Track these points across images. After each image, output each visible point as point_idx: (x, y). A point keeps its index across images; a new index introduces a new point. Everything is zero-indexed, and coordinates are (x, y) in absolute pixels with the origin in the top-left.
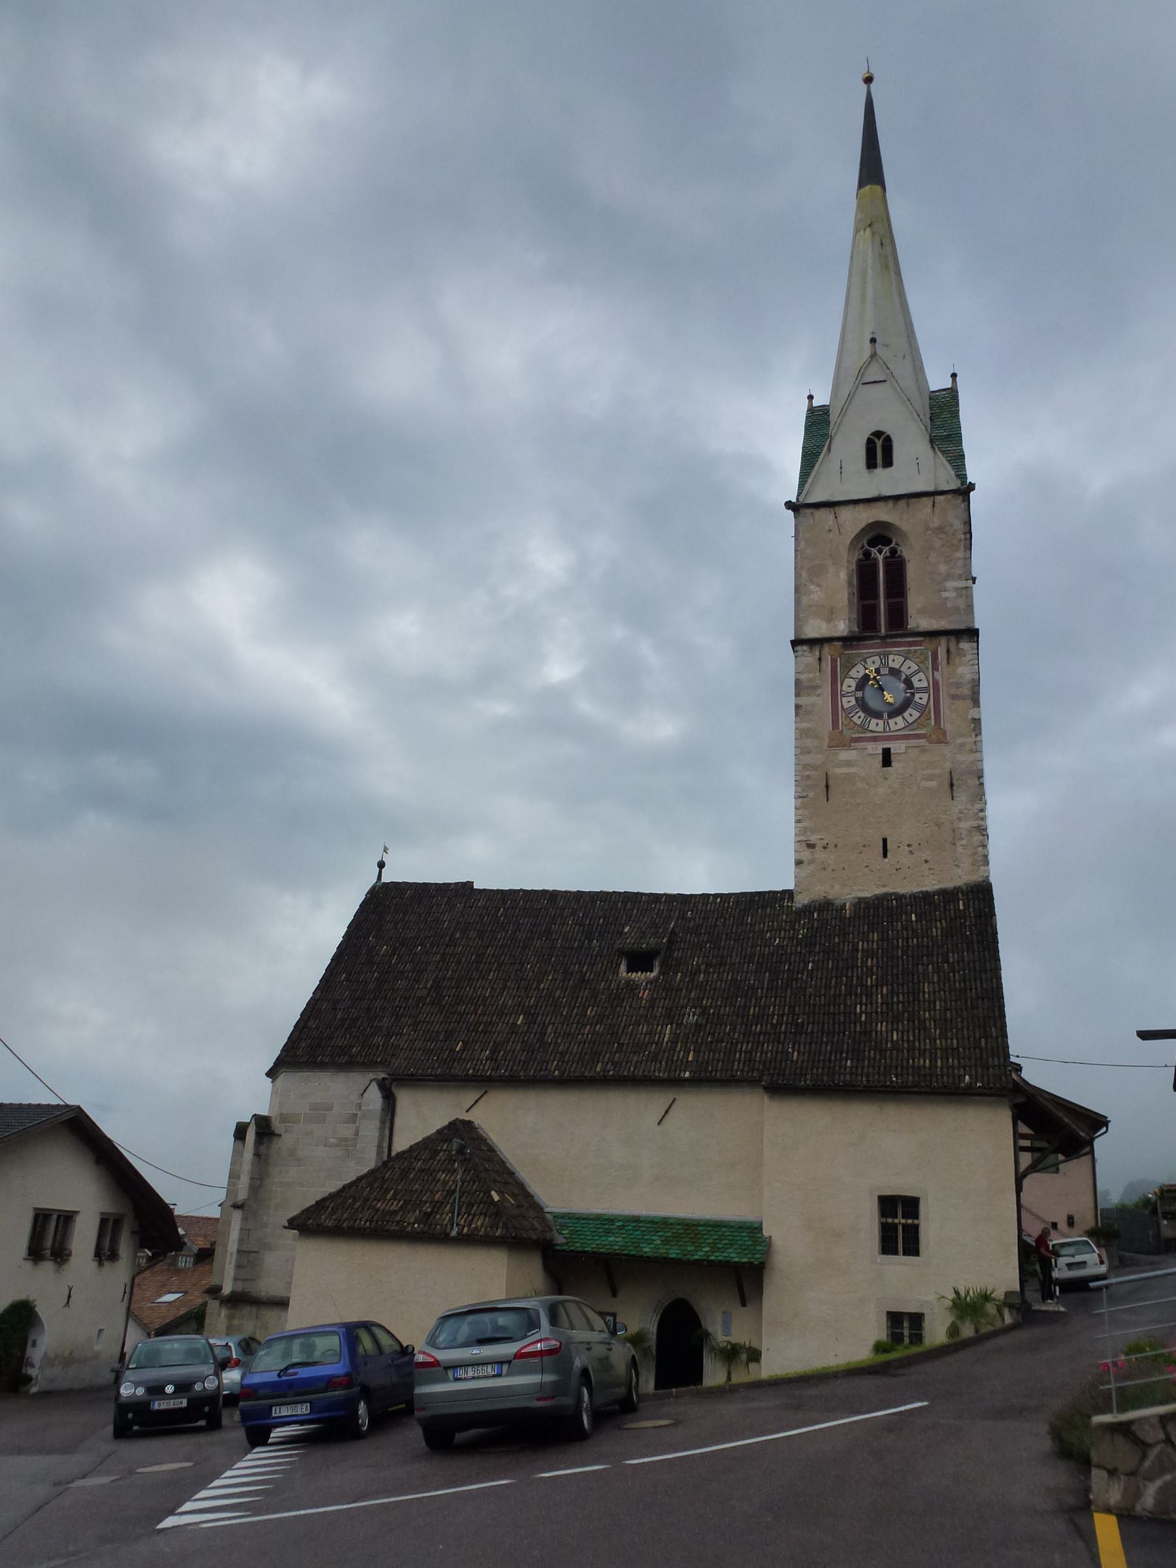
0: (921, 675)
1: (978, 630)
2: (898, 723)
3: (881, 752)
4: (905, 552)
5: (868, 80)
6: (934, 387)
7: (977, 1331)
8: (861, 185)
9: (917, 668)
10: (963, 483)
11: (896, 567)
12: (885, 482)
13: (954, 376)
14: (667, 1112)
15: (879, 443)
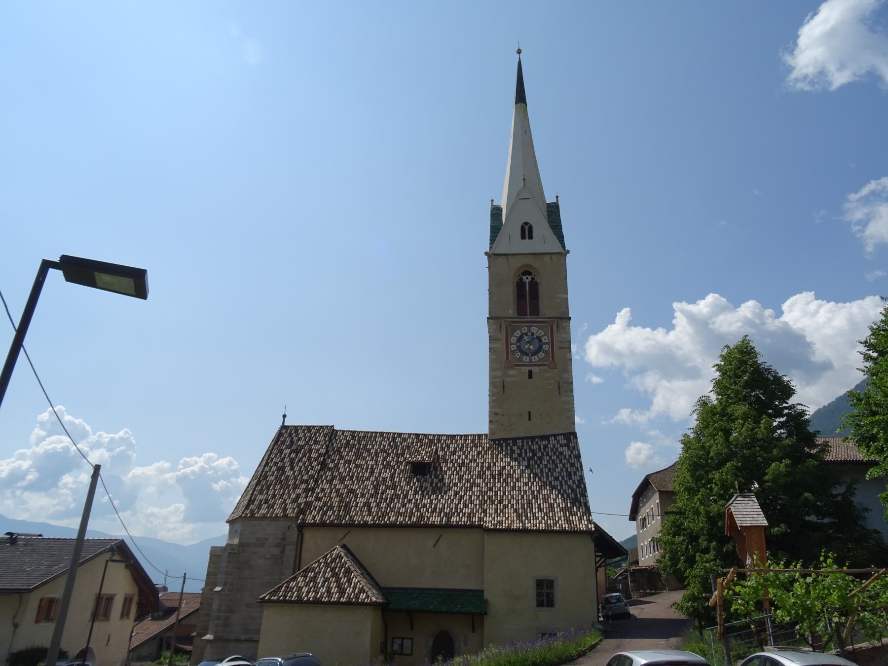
0: (546, 337)
1: (571, 317)
2: (535, 359)
3: (528, 371)
4: (537, 279)
5: (519, 52)
6: (548, 201)
8: (516, 103)
9: (544, 333)
10: (565, 249)
11: (534, 285)
12: (527, 246)
13: (557, 197)
14: (438, 541)
15: (527, 228)
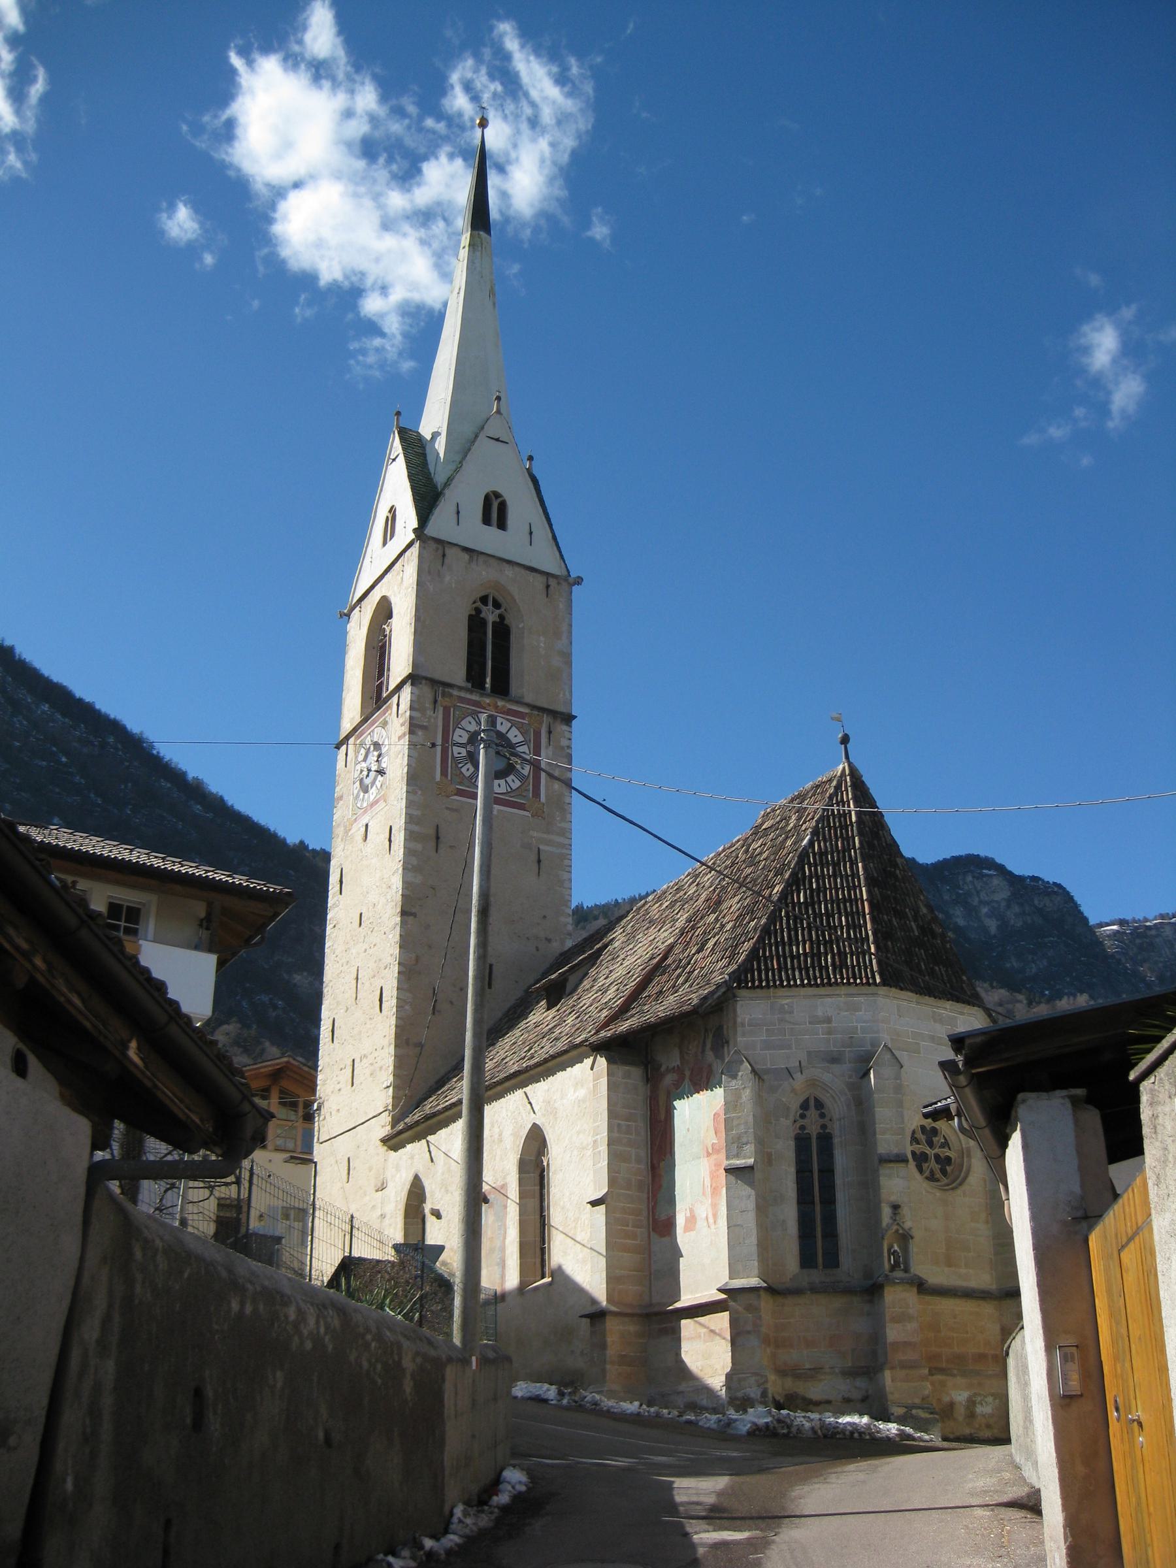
11: (503, 632)
12: (488, 539)
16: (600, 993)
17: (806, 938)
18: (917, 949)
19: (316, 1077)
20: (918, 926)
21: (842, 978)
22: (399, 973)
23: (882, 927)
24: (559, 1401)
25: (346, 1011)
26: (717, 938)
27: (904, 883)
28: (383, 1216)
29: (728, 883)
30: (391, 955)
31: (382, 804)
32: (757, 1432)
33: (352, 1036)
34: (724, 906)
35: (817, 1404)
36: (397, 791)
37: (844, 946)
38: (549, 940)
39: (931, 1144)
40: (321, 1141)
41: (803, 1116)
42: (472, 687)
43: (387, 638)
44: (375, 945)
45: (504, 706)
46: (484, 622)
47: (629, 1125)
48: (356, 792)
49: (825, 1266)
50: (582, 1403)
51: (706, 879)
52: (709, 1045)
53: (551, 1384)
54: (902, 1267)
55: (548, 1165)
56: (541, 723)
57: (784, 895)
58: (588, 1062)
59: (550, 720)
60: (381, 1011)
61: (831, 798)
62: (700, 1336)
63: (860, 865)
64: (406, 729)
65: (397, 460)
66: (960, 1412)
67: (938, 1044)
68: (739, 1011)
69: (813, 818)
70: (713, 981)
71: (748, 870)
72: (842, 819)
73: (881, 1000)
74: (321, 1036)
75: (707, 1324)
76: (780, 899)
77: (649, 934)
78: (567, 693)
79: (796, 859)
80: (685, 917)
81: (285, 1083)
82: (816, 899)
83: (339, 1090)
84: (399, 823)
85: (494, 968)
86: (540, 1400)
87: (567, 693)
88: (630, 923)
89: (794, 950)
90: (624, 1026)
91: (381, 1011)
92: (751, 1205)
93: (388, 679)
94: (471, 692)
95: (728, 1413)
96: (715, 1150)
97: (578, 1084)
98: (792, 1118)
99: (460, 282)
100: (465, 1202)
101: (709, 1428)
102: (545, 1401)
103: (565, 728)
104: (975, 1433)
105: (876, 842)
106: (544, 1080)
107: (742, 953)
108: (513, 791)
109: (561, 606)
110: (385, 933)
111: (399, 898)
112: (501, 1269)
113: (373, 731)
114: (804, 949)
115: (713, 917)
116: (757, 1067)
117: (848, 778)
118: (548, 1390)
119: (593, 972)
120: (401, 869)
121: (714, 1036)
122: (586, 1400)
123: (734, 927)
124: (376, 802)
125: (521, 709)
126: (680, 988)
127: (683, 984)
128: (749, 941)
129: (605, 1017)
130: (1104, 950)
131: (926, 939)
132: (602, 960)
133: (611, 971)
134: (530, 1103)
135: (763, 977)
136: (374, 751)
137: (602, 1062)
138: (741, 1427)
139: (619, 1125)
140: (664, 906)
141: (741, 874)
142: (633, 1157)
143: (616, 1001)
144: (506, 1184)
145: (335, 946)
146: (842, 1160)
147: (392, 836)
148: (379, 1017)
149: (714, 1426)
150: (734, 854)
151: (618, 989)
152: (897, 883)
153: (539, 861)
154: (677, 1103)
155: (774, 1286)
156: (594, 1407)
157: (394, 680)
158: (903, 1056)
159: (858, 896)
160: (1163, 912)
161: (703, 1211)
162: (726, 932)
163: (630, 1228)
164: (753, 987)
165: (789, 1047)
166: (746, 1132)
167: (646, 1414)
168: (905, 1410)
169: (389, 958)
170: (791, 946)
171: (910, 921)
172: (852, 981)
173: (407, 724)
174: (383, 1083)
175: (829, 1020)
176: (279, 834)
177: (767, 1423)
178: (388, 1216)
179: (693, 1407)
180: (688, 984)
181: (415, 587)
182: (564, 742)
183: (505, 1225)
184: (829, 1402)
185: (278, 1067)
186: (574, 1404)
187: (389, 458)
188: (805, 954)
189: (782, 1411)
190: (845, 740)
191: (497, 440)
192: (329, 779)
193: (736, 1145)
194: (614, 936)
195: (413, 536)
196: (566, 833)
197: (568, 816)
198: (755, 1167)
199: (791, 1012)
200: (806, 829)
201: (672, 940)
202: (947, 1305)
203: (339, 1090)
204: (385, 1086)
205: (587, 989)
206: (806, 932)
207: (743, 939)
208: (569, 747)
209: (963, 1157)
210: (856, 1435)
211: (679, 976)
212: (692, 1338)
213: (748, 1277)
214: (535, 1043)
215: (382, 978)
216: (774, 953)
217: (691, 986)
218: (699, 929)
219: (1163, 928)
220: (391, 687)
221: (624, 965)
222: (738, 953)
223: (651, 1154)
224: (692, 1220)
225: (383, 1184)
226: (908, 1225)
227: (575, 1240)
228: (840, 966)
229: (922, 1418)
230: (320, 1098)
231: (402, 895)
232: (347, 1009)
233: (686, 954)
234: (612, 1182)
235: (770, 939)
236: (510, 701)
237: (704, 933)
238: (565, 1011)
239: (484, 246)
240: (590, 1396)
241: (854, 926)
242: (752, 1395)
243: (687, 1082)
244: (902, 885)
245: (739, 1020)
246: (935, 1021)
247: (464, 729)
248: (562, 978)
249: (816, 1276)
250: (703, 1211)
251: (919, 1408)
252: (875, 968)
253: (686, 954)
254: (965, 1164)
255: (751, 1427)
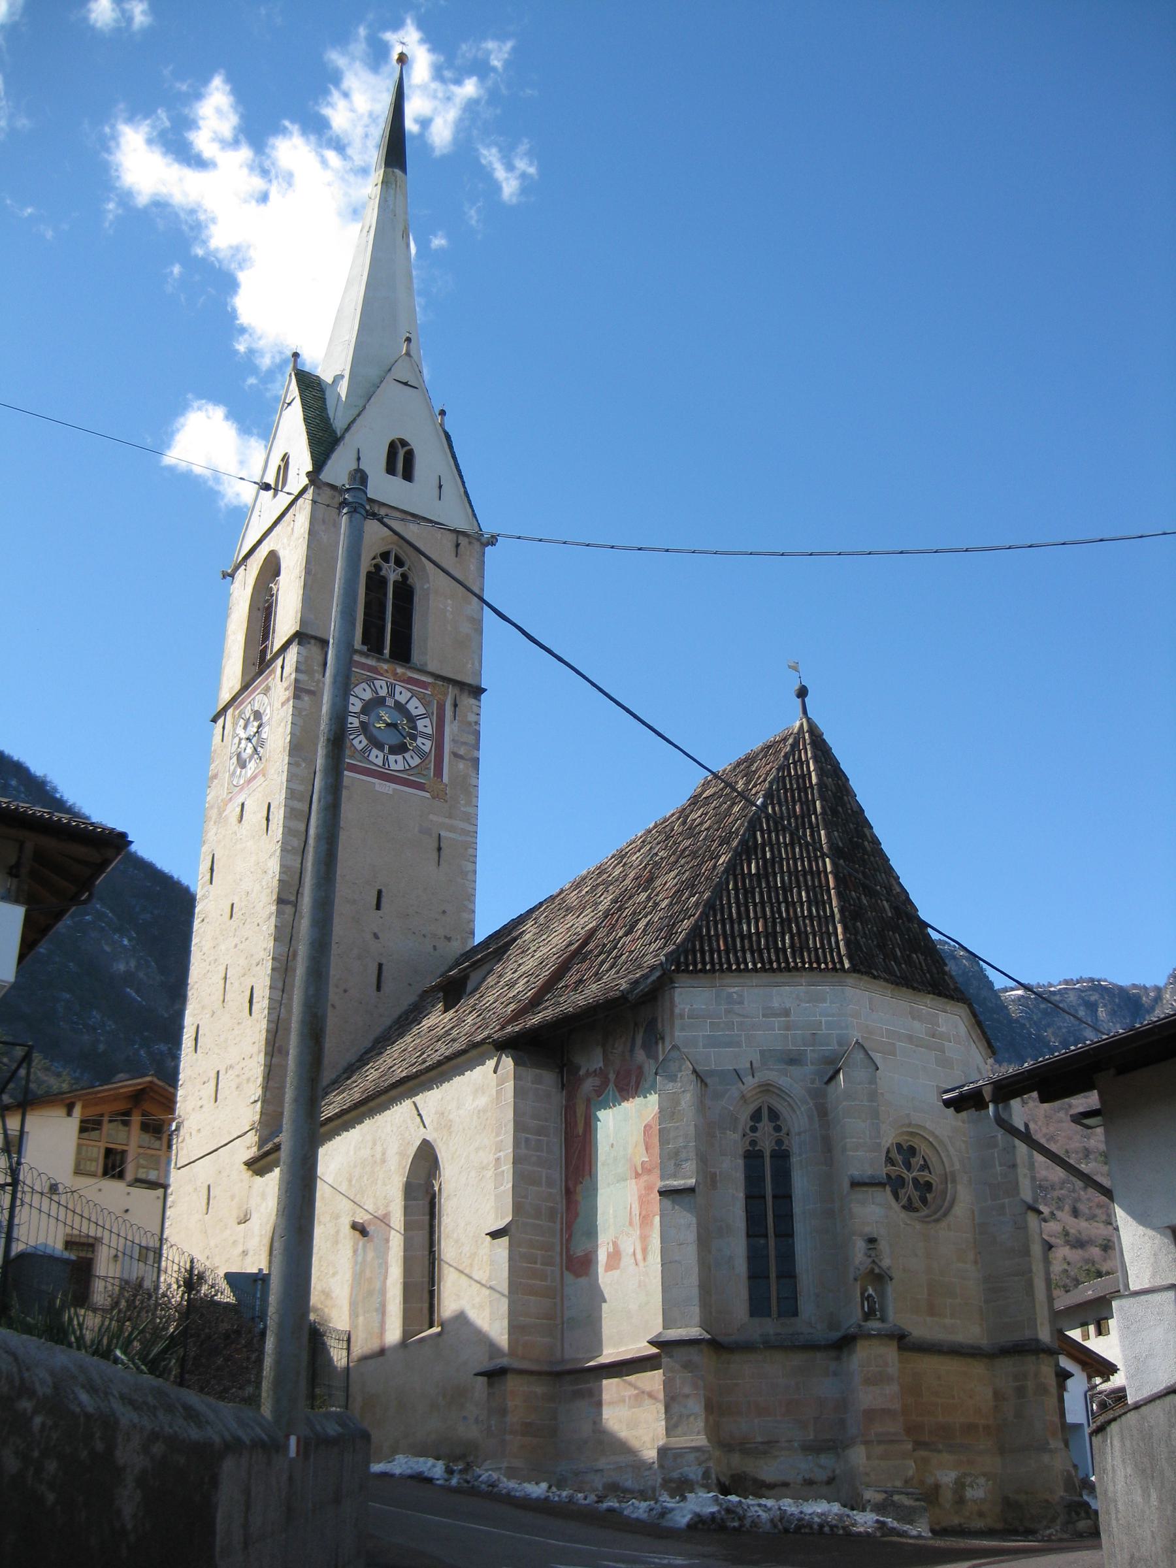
7: (99, 1277)
11: (405, 594)
15: (401, 453)
16: (507, 987)
17: (759, 914)
18: (891, 933)
19: (174, 1095)
20: (890, 906)
21: (804, 963)
22: (273, 969)
23: (850, 905)
24: (446, 1480)
25: (212, 1016)
26: (649, 917)
27: (875, 858)
28: (245, 1253)
29: (662, 858)
30: (265, 949)
31: (260, 779)
32: (700, 1526)
33: (217, 1045)
34: (658, 883)
35: (771, 1486)
36: (278, 763)
37: (805, 926)
38: (449, 939)
39: (909, 1167)
40: (178, 1166)
41: (754, 1129)
42: (368, 650)
43: (274, 597)
44: (246, 939)
45: (404, 674)
46: (383, 581)
47: (539, 1140)
48: (232, 768)
49: (780, 1315)
50: (476, 1483)
51: (634, 858)
52: (639, 1042)
53: (438, 1459)
54: (878, 1316)
55: (440, 1189)
56: (446, 694)
57: (732, 868)
58: (491, 1064)
59: (457, 691)
60: (251, 1014)
61: (786, 757)
62: (624, 1401)
63: (822, 832)
64: (290, 693)
65: (292, 404)
66: (947, 1496)
67: (917, 1046)
68: (677, 999)
69: (765, 781)
70: (645, 965)
71: (687, 843)
72: (801, 781)
73: (849, 991)
74: (183, 1046)
75: (639, 1384)
76: (726, 871)
77: (566, 922)
78: (477, 664)
79: (746, 824)
80: (609, 899)
81: (147, 1106)
82: (770, 870)
83: (201, 1107)
84: (279, 799)
85: (384, 968)
86: (422, 1479)
87: (477, 664)
88: (542, 914)
89: (745, 928)
90: (535, 1020)
91: (251, 1014)
92: (691, 1236)
93: (273, 642)
94: (367, 656)
95: (661, 1499)
96: (647, 1169)
97: (478, 1090)
98: (740, 1132)
99: (372, 218)
100: (288, 1183)
101: (637, 1519)
102: (429, 1480)
103: (473, 701)
104: (964, 1524)
105: (840, 809)
106: (438, 1088)
107: (681, 932)
108: (411, 768)
109: (472, 567)
110: (258, 925)
111: (276, 883)
112: (380, 1316)
113: (254, 699)
114: (757, 927)
115: (644, 896)
116: (698, 1068)
117: (807, 735)
118: (434, 1466)
119: (498, 968)
120: (279, 851)
121: (645, 1031)
122: (480, 1479)
123: (670, 904)
124: (254, 778)
125: (424, 678)
126: (604, 975)
127: (607, 971)
128: (689, 919)
129: (512, 1011)
130: (1008, 1014)
131: (900, 921)
132: (510, 955)
133: (520, 965)
134: (419, 1115)
135: (707, 959)
136: (253, 721)
137: (508, 1063)
138: (678, 1518)
139: (527, 1140)
140: (584, 892)
141: (677, 848)
142: (544, 1180)
143: (526, 993)
144: (389, 1212)
145: (203, 943)
146: (802, 1183)
147: (271, 813)
148: (248, 1021)
149: (644, 1516)
150: (668, 828)
151: (529, 981)
152: (866, 857)
153: (439, 849)
154: (601, 1114)
155: (720, 1338)
156: (490, 1488)
157: (278, 640)
158: (877, 1057)
159: (821, 869)
160: (1068, 978)
161: (630, 1244)
162: (660, 911)
163: (538, 1266)
164: (695, 971)
165: (739, 1045)
166: (685, 1147)
167: (556, 1499)
168: (884, 1496)
169: (262, 953)
170: (740, 923)
171: (882, 901)
172: (815, 965)
173: (292, 688)
174: (250, 1097)
175: (787, 1013)
176: (183, 882)
177: (713, 1514)
178: (251, 1253)
179: (614, 1489)
180: (614, 970)
181: (307, 536)
182: (472, 718)
183: (386, 1263)
184: (786, 1485)
185: (139, 1087)
186: (466, 1485)
187: (284, 402)
188: (758, 933)
189: (729, 1497)
190: (802, 693)
191: (406, 384)
192: (206, 755)
193: (672, 1162)
194: (524, 929)
195: (306, 481)
196: (471, 819)
197: (474, 800)
198: (697, 1189)
199: (741, 1003)
200: (757, 793)
201: (594, 923)
202: (929, 1365)
203: (201, 1107)
204: (252, 1100)
205: (492, 986)
206: (758, 909)
207: (681, 917)
208: (477, 723)
209: (946, 1183)
210: (826, 1529)
211: (603, 962)
212: (613, 1403)
213: (687, 1326)
214: (428, 1047)
215: (254, 976)
216: (720, 932)
217: (617, 972)
218: (627, 910)
219: (1067, 993)
220: (275, 649)
221: (536, 957)
222: (676, 933)
223: (566, 1176)
224: (615, 1257)
225: (246, 1215)
226: (886, 1262)
227: (471, 1278)
228: (800, 948)
229: (906, 1506)
230: (180, 1117)
231: (279, 880)
232: (214, 1013)
233: (611, 938)
234: (517, 1208)
235: (715, 916)
236: (410, 668)
237: (634, 913)
238: (465, 1011)
239: (398, 184)
240: (486, 1474)
241: (818, 901)
242: (692, 1476)
243: (611, 1086)
244: (872, 859)
245: (677, 1011)
246: (913, 1018)
247: (357, 697)
248: (462, 974)
249: (770, 1327)
250: (630, 1244)
251: (902, 1493)
252: (843, 951)
253: (611, 938)
254: (949, 1191)
255: (692, 1519)
